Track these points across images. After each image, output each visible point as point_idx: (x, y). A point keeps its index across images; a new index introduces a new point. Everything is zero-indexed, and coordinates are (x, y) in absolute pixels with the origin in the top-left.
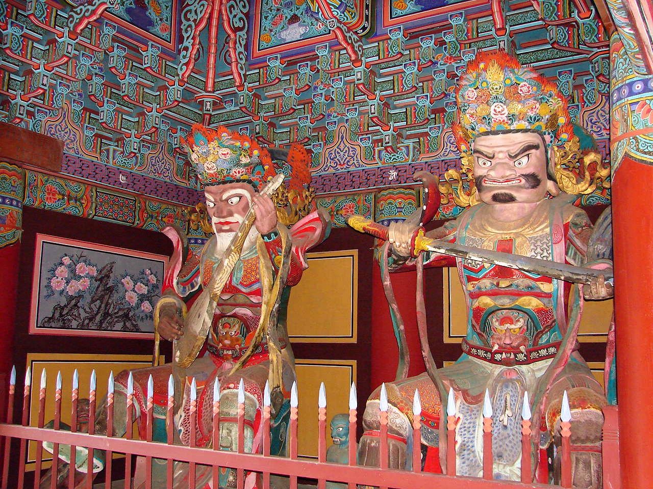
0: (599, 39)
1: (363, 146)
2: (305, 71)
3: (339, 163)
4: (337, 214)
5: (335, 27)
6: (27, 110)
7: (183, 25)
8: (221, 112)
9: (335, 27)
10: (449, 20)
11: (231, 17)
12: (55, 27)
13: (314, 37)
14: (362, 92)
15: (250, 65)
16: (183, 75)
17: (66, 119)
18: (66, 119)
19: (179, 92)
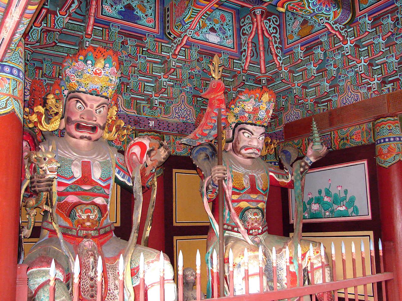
0: (156, 51)
1: (361, 92)
2: (318, 51)
3: (181, 116)
4: (351, 138)
5: (325, 23)
6: (159, 102)
7: (242, 38)
8: (274, 84)
9: (325, 23)
10: (395, 3)
11: (267, 28)
12: (161, 53)
13: (318, 31)
14: (352, 60)
15: (284, 54)
16: (244, 66)
17: (350, 90)
18: (350, 90)
19: (314, 70)
